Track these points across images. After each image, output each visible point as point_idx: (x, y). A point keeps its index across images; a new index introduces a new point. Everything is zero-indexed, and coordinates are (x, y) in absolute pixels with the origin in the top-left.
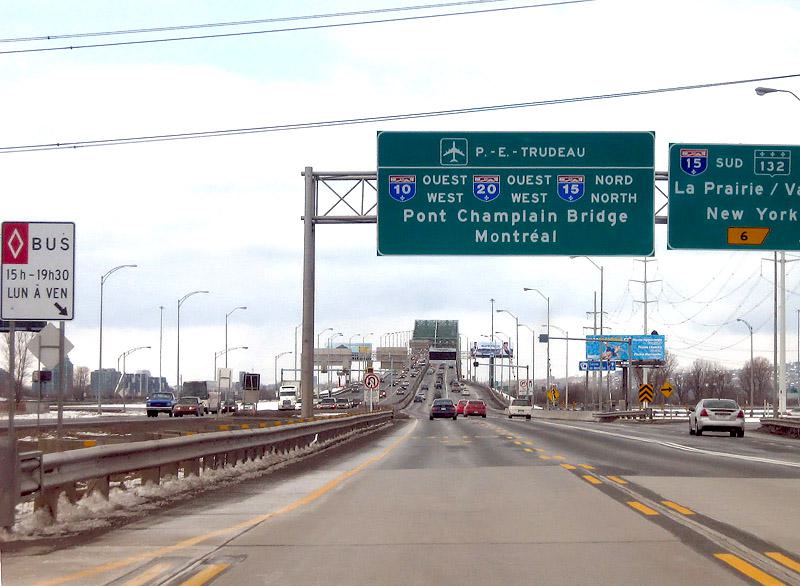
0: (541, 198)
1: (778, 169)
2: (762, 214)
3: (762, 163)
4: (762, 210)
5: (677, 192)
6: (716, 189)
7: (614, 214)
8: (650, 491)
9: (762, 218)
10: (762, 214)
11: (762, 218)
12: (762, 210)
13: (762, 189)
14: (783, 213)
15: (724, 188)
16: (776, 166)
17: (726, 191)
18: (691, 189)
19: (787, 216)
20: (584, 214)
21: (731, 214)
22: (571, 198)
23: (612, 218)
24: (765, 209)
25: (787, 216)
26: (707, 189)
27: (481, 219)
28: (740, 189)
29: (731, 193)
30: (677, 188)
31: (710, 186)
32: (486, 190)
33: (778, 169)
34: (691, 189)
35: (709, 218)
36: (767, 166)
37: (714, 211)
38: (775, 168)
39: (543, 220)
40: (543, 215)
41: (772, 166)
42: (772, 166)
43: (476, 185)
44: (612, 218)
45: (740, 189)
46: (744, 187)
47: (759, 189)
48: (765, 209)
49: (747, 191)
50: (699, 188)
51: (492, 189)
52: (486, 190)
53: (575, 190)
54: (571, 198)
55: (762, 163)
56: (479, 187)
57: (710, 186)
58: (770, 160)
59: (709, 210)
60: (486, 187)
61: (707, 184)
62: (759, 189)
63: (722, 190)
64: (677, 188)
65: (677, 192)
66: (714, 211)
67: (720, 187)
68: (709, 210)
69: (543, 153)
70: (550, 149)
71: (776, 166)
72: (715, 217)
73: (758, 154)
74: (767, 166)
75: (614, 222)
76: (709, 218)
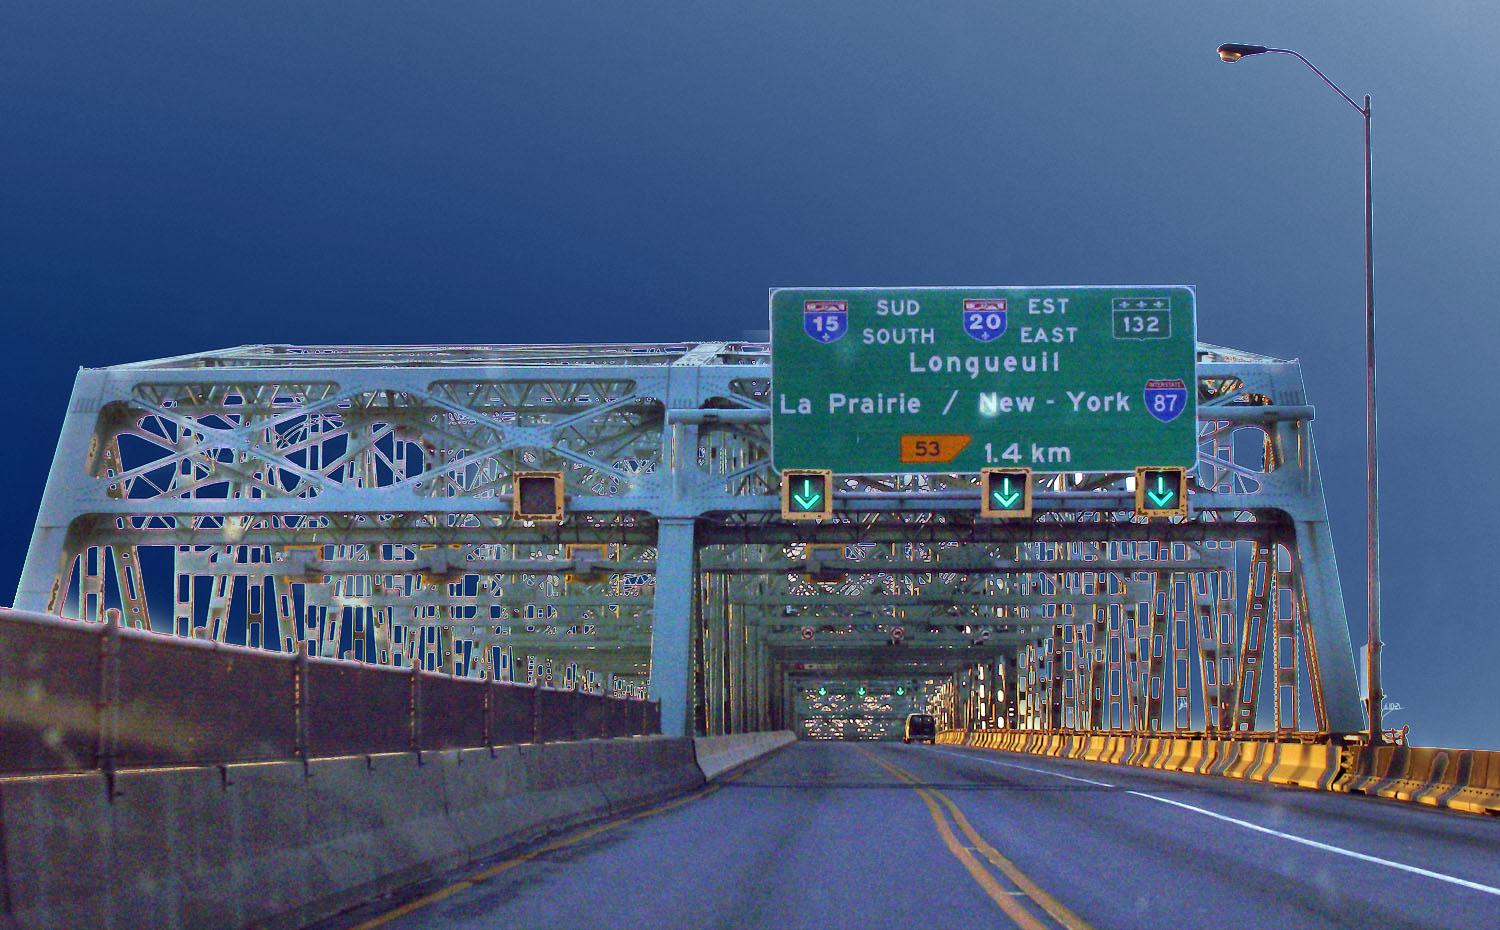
0: (1066, 335)
1: (1150, 329)
2: (1076, 401)
3: (1127, 320)
4: (1076, 396)
5: (784, 410)
6: (847, 405)
8: (1327, 757)
9: (1076, 408)
10: (1076, 401)
11: (1076, 408)
12: (1076, 396)
13: (918, 404)
14: (1108, 399)
15: (861, 403)
16: (1146, 324)
17: (863, 408)
18: (806, 406)
19: (1113, 404)
20: (890, 401)
21: (1015, 402)
25: (1113, 404)
26: (833, 406)
27: (1019, 361)
28: (885, 404)
29: (871, 410)
30: (783, 403)
31: (839, 400)
32: (984, 323)
33: (1150, 329)
34: (806, 406)
36: (1134, 324)
39: (1045, 369)
40: (1044, 359)
41: (1140, 324)
42: (1140, 324)
43: (968, 316)
45: (885, 404)
47: (914, 405)
48: (1082, 394)
49: (896, 406)
50: (820, 404)
51: (993, 322)
52: (984, 323)
55: (1127, 320)
56: (972, 319)
57: (839, 400)
60: (985, 319)
61: (832, 396)
62: (914, 405)
64: (783, 403)
65: (784, 410)
67: (853, 401)
69: (898, 309)
70: (909, 302)
71: (1146, 324)
74: (1134, 324)
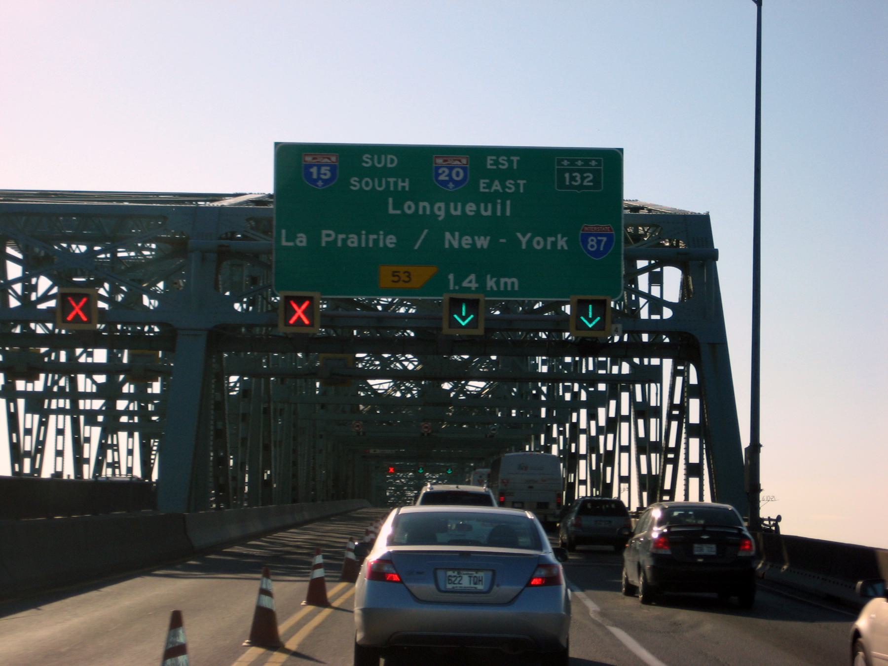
2: (524, 241)
3: (567, 175)
4: (524, 236)
5: (284, 243)
6: (336, 239)
7: (442, 205)
9: (524, 247)
11: (524, 247)
12: (524, 236)
14: (550, 239)
15: (347, 238)
19: (554, 244)
21: (473, 240)
22: (320, 183)
23: (439, 209)
24: (529, 235)
25: (554, 244)
26: (324, 240)
28: (367, 240)
33: (585, 183)
35: (447, 246)
36: (573, 179)
37: (450, 243)
38: (582, 182)
41: (578, 178)
42: (578, 178)
44: (439, 209)
45: (367, 240)
46: (372, 237)
47: (391, 241)
48: (529, 235)
49: (376, 241)
53: (326, 173)
54: (320, 183)
55: (567, 175)
58: (575, 171)
59: (448, 235)
62: (391, 241)
63: (344, 241)
66: (453, 236)
67: (341, 236)
68: (448, 235)
71: (583, 179)
72: (456, 245)
73: (559, 162)
74: (573, 179)
75: (442, 214)
76: (447, 246)
